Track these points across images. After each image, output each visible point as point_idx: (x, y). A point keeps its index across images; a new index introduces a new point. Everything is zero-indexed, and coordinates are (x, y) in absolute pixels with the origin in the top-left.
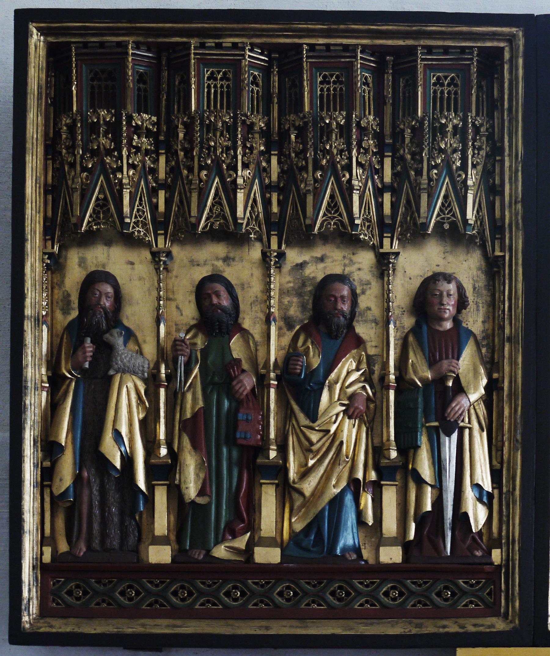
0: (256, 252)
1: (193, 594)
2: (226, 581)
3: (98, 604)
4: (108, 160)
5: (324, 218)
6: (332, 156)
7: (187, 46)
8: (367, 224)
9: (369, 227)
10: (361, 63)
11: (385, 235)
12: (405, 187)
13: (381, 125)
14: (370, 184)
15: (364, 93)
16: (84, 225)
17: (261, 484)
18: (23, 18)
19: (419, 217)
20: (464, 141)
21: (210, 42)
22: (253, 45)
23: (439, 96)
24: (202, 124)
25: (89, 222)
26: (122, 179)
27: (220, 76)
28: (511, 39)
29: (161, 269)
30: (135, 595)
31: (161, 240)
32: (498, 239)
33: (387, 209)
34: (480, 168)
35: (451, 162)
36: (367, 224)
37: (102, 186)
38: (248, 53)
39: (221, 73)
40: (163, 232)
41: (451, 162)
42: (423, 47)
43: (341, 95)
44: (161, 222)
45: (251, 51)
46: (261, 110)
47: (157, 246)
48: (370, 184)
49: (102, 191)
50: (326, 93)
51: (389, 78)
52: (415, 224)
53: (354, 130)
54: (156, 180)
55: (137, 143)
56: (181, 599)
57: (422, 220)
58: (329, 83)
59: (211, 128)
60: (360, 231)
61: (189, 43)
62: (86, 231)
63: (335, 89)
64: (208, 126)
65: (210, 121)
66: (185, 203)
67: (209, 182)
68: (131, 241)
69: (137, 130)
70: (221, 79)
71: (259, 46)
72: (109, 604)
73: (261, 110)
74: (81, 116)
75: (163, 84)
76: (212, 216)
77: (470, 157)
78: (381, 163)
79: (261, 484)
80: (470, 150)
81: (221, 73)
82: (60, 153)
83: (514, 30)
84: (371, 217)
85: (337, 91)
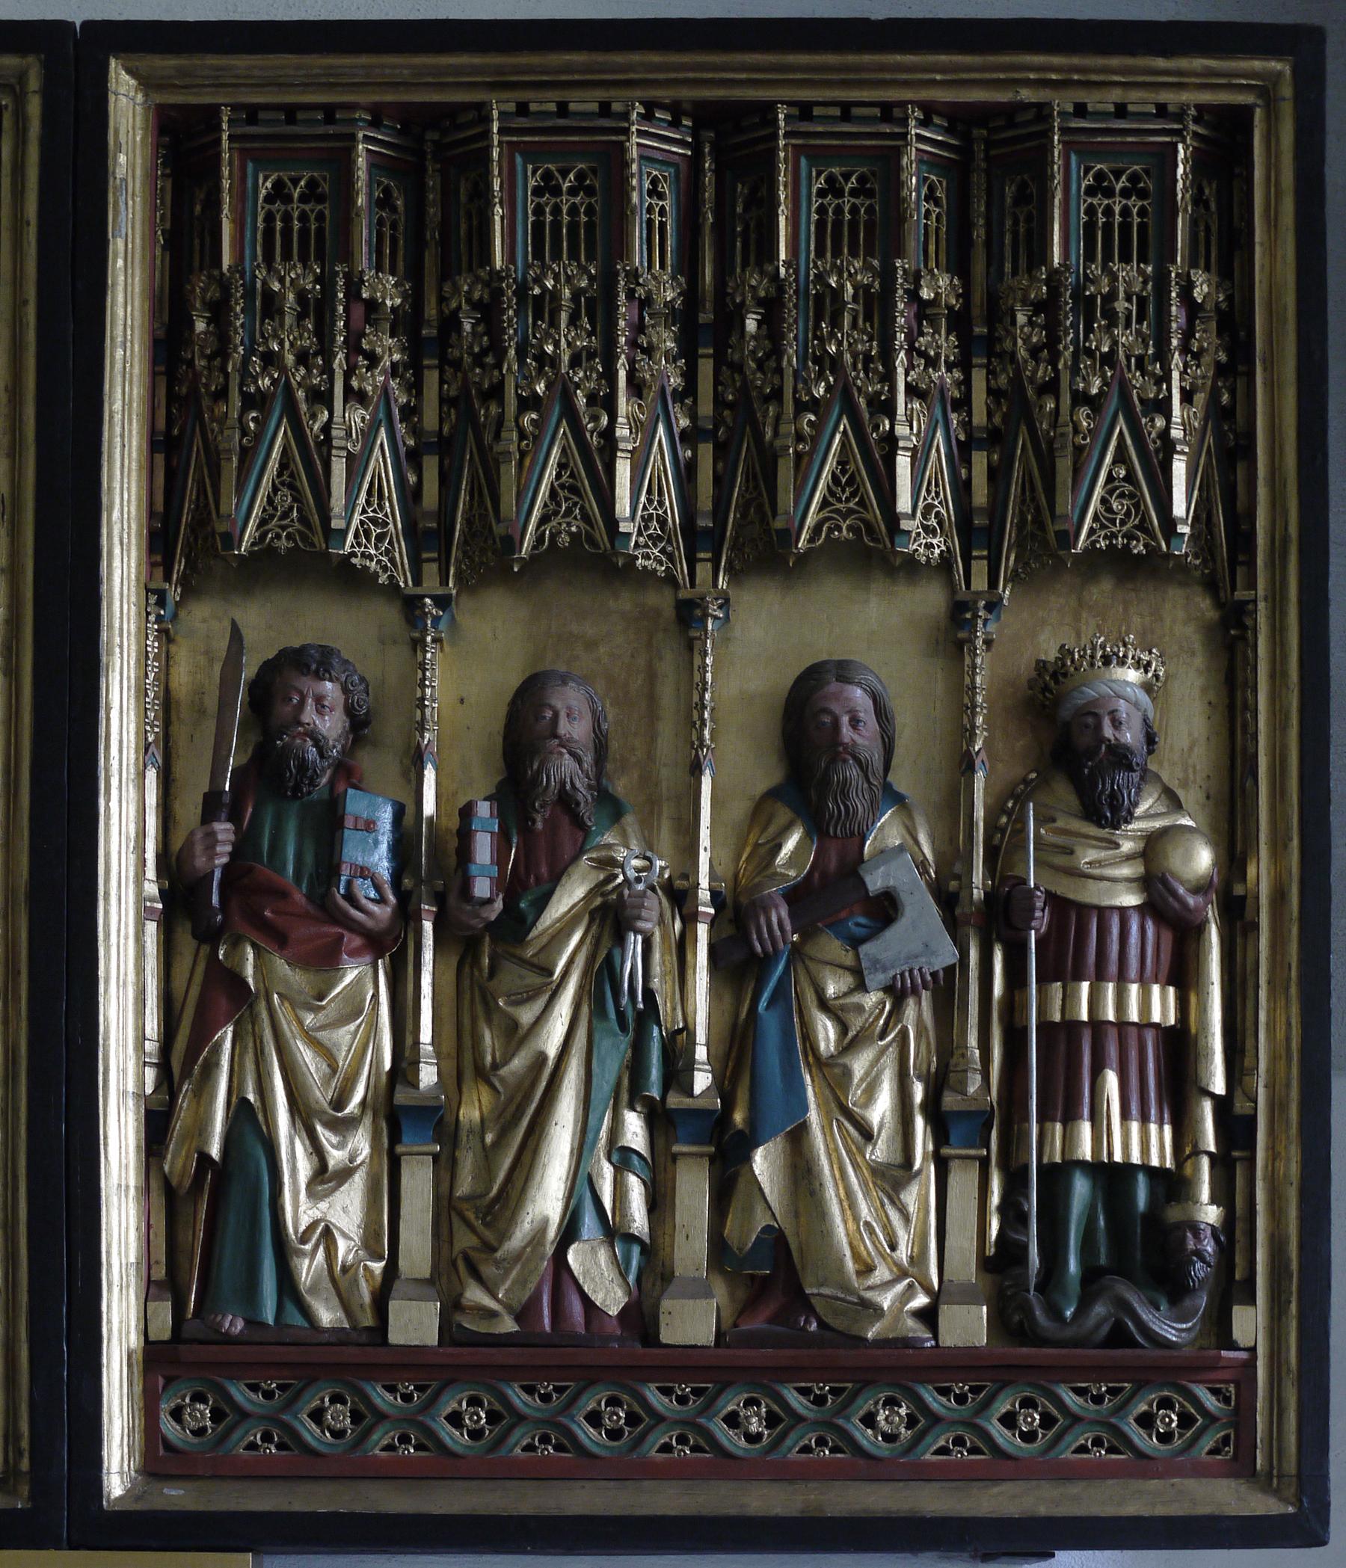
0: (928, 600)
1: (1055, 1421)
2: (1140, 1386)
3: (1082, 1449)
4: (1137, 379)
5: (821, 515)
6: (283, 369)
7: (481, 114)
8: (375, 531)
9: (380, 538)
10: (917, 149)
11: (425, 555)
12: (457, 445)
13: (966, 296)
14: (939, 436)
15: (926, 218)
16: (1083, 537)
17: (675, 1158)
18: (1301, 44)
19: (775, 514)
20: (323, 334)
21: (544, 102)
22: (650, 107)
23: (296, 228)
24: (249, 294)
25: (1092, 531)
26: (1168, 428)
27: (1120, 185)
28: (1267, 92)
29: (429, 639)
30: (1178, 1426)
31: (703, 571)
32: (1242, 563)
33: (980, 495)
34: (1200, 398)
35: (572, 387)
36: (375, 531)
37: (1121, 446)
38: (1192, 127)
39: (572, 176)
40: (709, 555)
41: (572, 387)
42: (235, 107)
43: (870, 226)
44: (428, 532)
45: (924, 123)
46: (400, 265)
47: (693, 584)
48: (939, 436)
49: (1121, 457)
50: (1137, 220)
51: (978, 180)
52: (767, 531)
53: (901, 306)
54: (415, 431)
55: (928, 345)
56: (1021, 1433)
57: (779, 524)
58: (1109, 193)
59: (545, 307)
60: (352, 546)
61: (1048, 105)
62: (1086, 550)
63: (854, 210)
64: (538, 300)
65: (543, 287)
66: (488, 488)
67: (817, 436)
68: (350, 579)
69: (924, 311)
70: (573, 191)
71: (677, 111)
72: (973, 1450)
73: (400, 265)
74: (242, 277)
75: (434, 200)
76: (272, 517)
77: (900, 371)
78: (966, 383)
79: (675, 1158)
80: (340, 356)
81: (572, 176)
82: (191, 363)
83: (1275, 65)
84: (665, 512)
85: (543, 213)
